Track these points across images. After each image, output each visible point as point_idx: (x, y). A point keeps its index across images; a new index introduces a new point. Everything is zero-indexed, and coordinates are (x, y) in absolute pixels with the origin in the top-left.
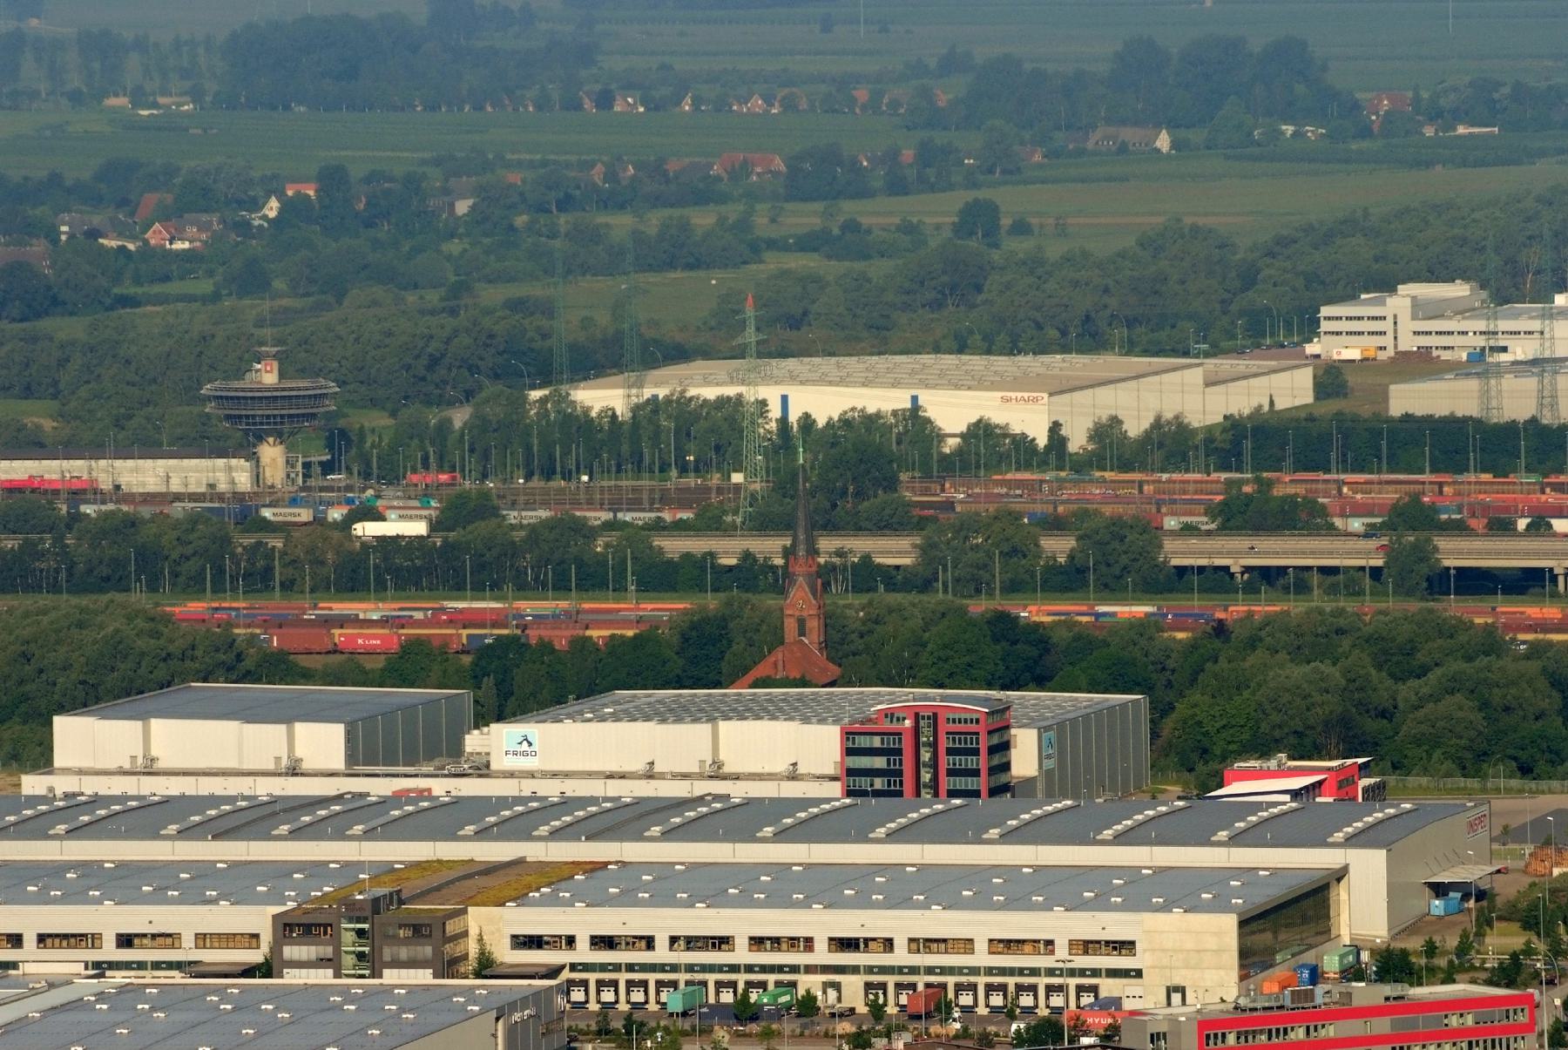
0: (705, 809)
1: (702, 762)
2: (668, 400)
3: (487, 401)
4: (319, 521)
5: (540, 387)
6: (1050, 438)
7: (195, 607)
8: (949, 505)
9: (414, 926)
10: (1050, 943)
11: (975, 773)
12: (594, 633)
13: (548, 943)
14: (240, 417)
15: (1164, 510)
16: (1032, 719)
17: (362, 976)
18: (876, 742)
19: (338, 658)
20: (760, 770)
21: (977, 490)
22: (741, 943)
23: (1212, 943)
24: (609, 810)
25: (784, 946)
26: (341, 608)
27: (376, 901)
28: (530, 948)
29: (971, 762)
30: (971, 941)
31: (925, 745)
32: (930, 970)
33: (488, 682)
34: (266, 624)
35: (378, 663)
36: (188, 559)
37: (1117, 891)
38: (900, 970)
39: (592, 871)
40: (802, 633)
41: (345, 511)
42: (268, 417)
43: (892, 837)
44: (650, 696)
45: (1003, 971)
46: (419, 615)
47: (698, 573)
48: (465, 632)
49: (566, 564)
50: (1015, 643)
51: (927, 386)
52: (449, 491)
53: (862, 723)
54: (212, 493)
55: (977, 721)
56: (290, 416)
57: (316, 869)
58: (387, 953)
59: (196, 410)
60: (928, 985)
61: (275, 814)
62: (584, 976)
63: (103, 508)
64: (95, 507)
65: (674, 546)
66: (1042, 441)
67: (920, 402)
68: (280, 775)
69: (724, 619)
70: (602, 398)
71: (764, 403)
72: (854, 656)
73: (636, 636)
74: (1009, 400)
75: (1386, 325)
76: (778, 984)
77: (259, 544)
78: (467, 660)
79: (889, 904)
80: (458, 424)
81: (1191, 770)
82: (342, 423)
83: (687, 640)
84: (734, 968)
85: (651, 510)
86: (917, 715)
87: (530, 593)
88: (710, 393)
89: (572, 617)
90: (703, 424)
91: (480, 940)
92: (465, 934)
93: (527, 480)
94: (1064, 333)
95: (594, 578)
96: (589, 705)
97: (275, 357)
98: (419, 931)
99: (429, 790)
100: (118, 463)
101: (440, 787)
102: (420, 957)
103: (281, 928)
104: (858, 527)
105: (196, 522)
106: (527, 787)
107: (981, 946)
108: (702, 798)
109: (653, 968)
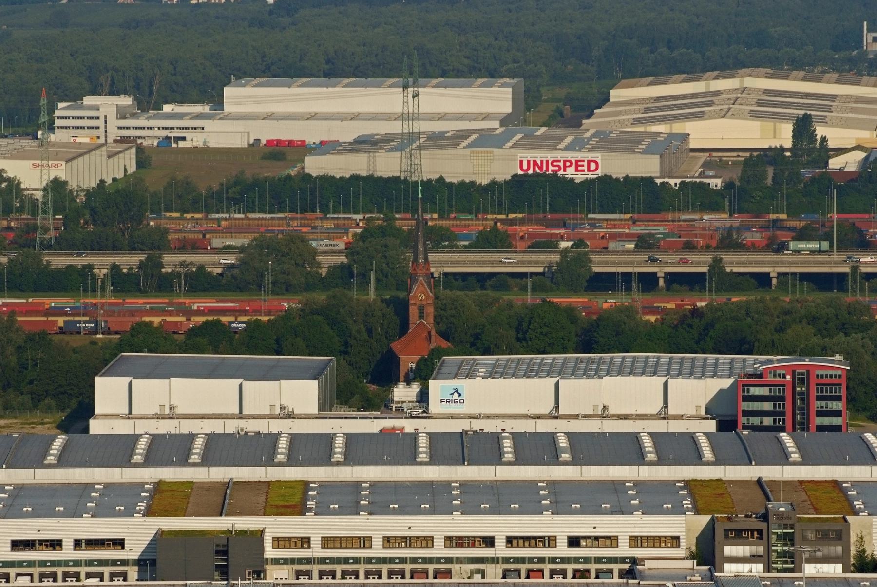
22: (377, 542)
25: (37, 546)
55: (840, 376)
62: (54, 569)
73: (269, 320)
74: (476, 152)
75: (100, 123)
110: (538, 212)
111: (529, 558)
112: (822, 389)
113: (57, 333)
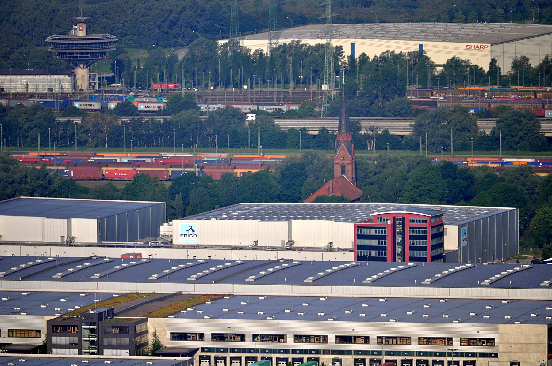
0: (278, 267)
1: (283, 241)
2: (290, 46)
4: (103, 109)
5: (223, 39)
6: (490, 68)
7: (33, 154)
9: (120, 327)
11: (424, 248)
13: (190, 337)
14: (66, 53)
15: (546, 107)
16: (456, 220)
17: (93, 353)
18: (373, 232)
19: (105, 182)
20: (313, 246)
21: (450, 95)
22: (290, 339)
23: (534, 339)
25: (312, 340)
26: (108, 156)
27: (100, 315)
29: (422, 243)
32: (388, 353)
34: (68, 164)
35: (121, 186)
36: (32, 129)
37: (487, 312)
38: (372, 353)
39: (215, 299)
40: (343, 172)
42: (80, 54)
44: (258, 206)
45: (426, 354)
46: (148, 160)
47: (300, 138)
48: (171, 170)
49: (230, 133)
50: (455, 179)
52: (174, 93)
54: (51, 93)
55: (426, 221)
56: (91, 53)
57: (72, 296)
58: (106, 341)
60: (387, 361)
61: (55, 267)
65: (285, 124)
66: (486, 69)
67: (424, 48)
68: (63, 245)
69: (303, 164)
70: (256, 45)
71: (341, 48)
72: (370, 185)
76: (309, 359)
78: (168, 184)
79: (492, 321)
80: (181, 57)
81: (541, 246)
83: (284, 176)
84: (286, 351)
86: (394, 218)
87: (209, 149)
88: (313, 42)
89: (229, 162)
90: (309, 59)
91: (155, 335)
92: (147, 332)
93: (215, 88)
94: (506, 11)
96: (226, 210)
97: (85, 22)
98: (122, 330)
99: (140, 255)
101: (145, 253)
102: (123, 344)
103: (51, 327)
104: (383, 115)
106: (191, 254)
107: (415, 341)
108: (278, 261)
109: (244, 350)
110: (289, 96)
112: (413, 231)
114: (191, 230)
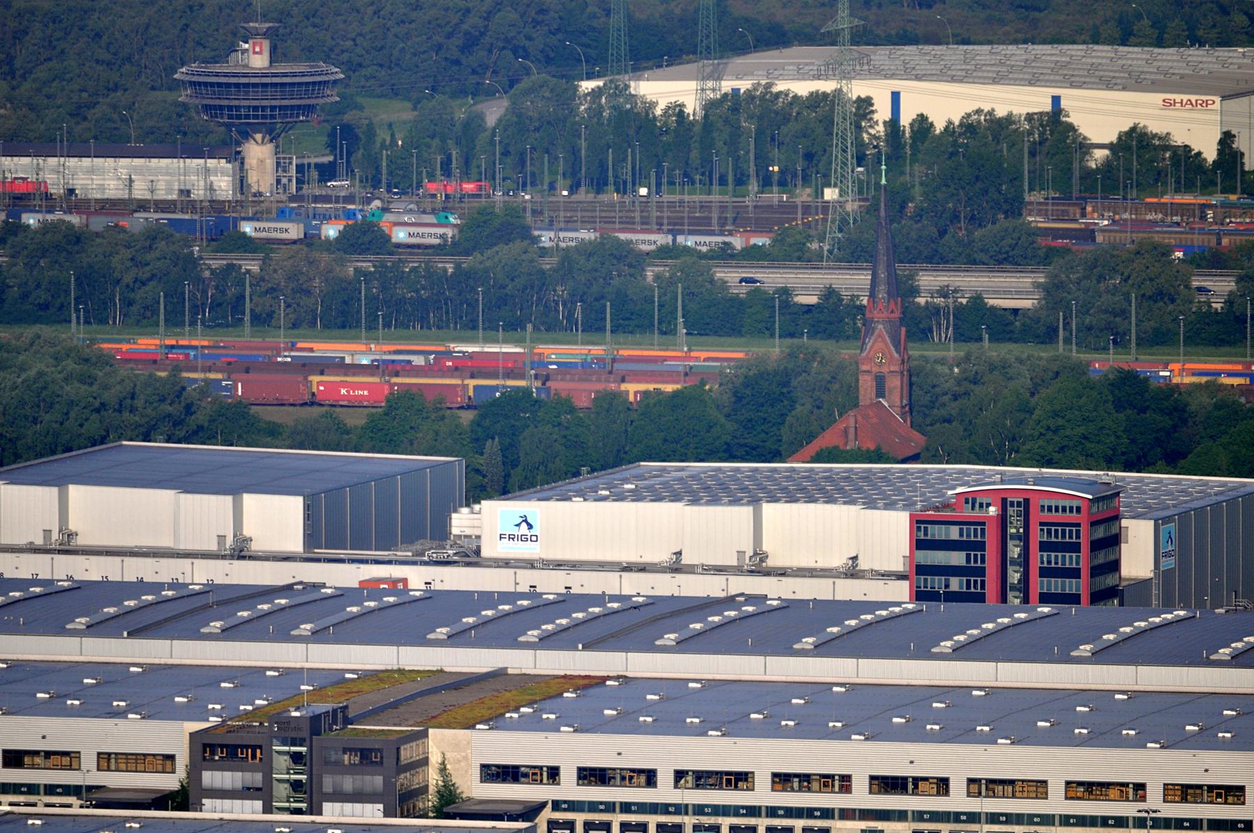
0: (732, 613)
1: (741, 553)
2: (750, 95)
3: (528, 92)
4: (310, 240)
6: (1220, 152)
7: (147, 343)
8: (1088, 234)
9: (362, 750)
10: (1140, 787)
11: (1075, 573)
12: (632, 389)
13: (526, 775)
14: (221, 107)
16: (1149, 507)
17: (298, 811)
18: (954, 533)
19: (316, 410)
20: (812, 565)
21: (1126, 216)
24: (616, 612)
25: (815, 785)
26: (324, 349)
28: (504, 781)
29: (1068, 560)
30: (1044, 783)
31: (1012, 537)
33: (492, 446)
34: (230, 368)
35: (356, 420)
36: (144, 284)
39: (586, 687)
41: (341, 228)
42: (255, 108)
43: (960, 653)
44: (682, 469)
46: (418, 360)
47: (778, 314)
49: (609, 300)
50: (1143, 410)
51: (1072, 86)
53: (936, 509)
54: (186, 200)
56: (281, 108)
57: (249, 677)
58: (328, 783)
59: (170, 96)
61: (206, 607)
62: (569, 816)
63: (50, 217)
64: (40, 216)
66: (1210, 155)
68: (224, 557)
70: (669, 92)
71: (865, 104)
72: (945, 424)
73: (675, 394)
77: (231, 267)
78: (467, 417)
80: (491, 119)
82: (348, 117)
85: (721, 234)
86: (1004, 501)
87: (560, 335)
88: (803, 88)
89: (608, 367)
90: (793, 127)
91: (443, 769)
92: (425, 762)
93: (571, 193)
95: (635, 317)
97: (265, 35)
98: (368, 756)
99: (405, 581)
100: (72, 162)
101: (417, 578)
102: (368, 789)
103: (200, 749)
104: (970, 260)
105: (155, 238)
106: (525, 580)
107: (1056, 789)
109: (654, 808)
111: (591, 803)
113: (462, 408)
114: (524, 524)
